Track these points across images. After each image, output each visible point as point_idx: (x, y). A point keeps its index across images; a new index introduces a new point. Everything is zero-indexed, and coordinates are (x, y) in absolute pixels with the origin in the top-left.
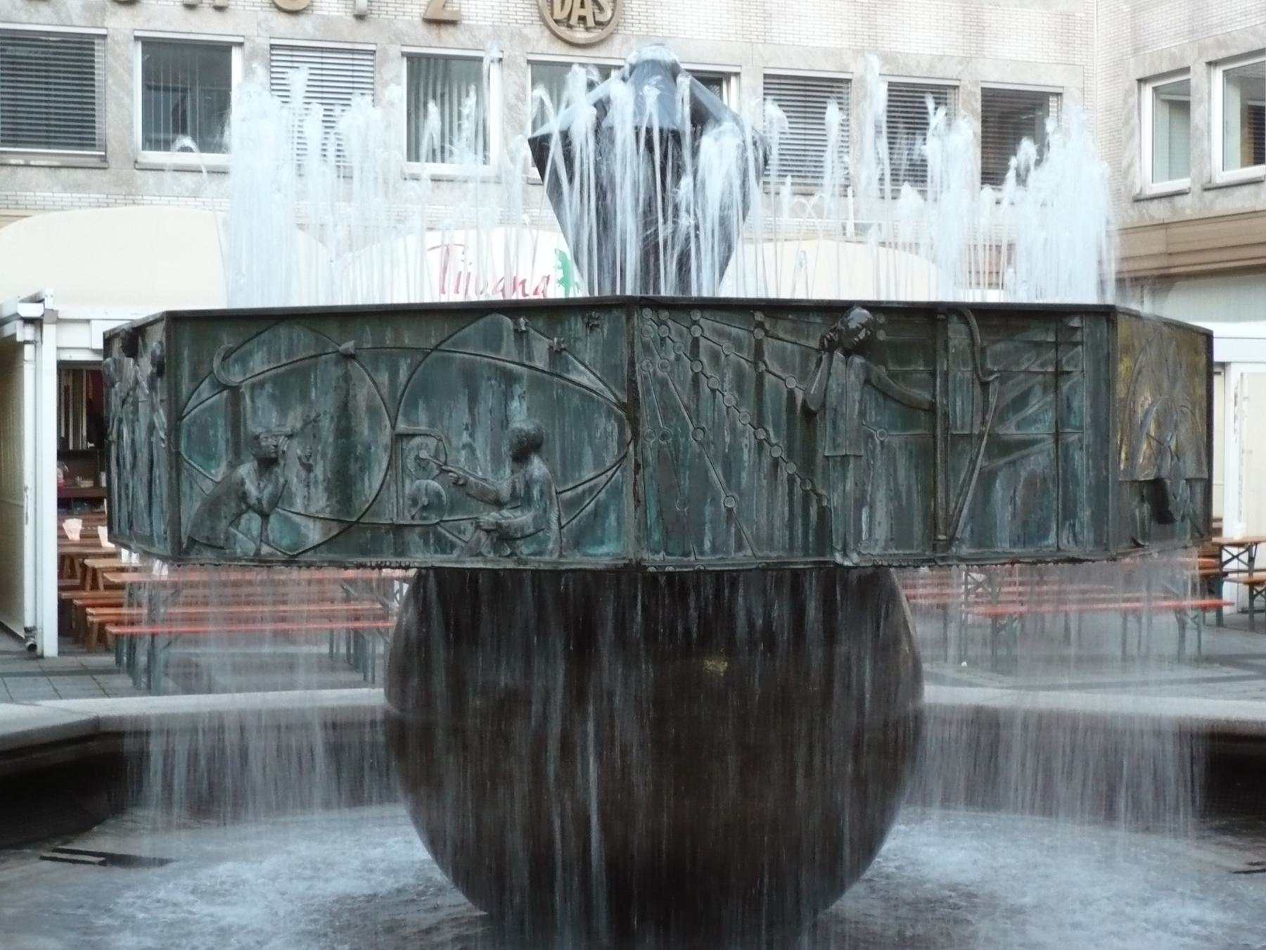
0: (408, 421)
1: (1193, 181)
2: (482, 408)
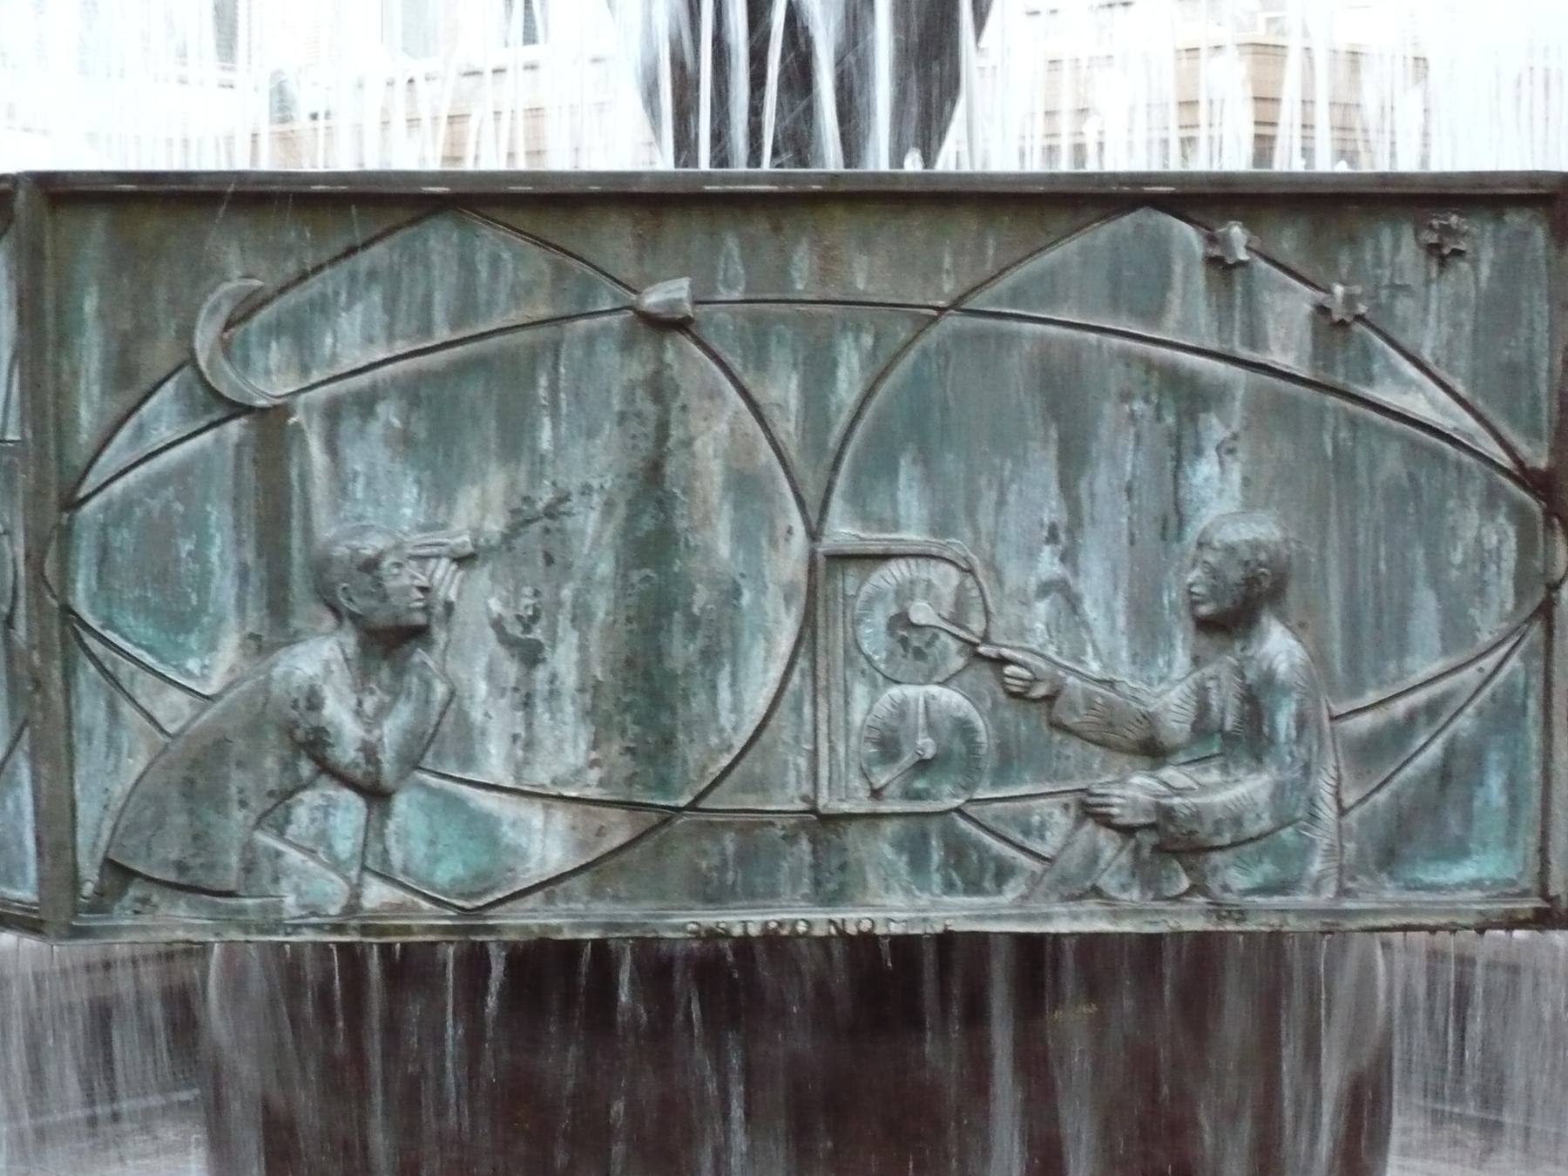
0: (865, 517)
2: (1102, 481)
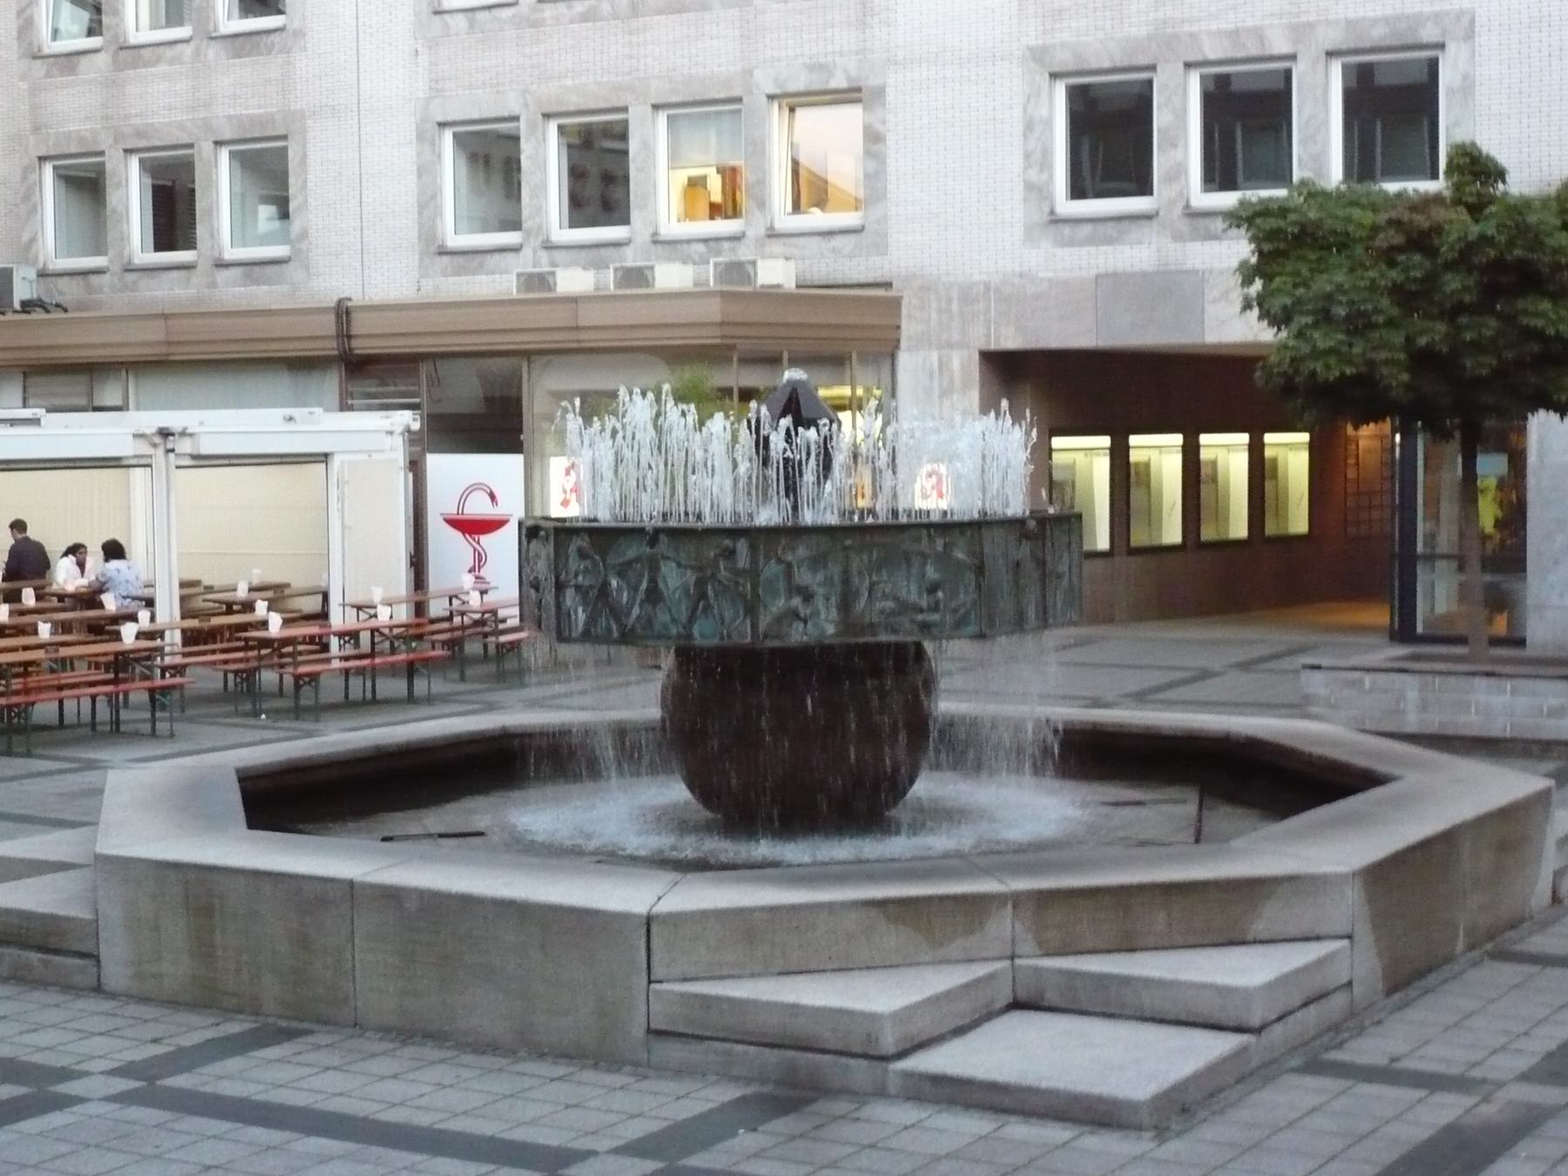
1: (111, 262)
